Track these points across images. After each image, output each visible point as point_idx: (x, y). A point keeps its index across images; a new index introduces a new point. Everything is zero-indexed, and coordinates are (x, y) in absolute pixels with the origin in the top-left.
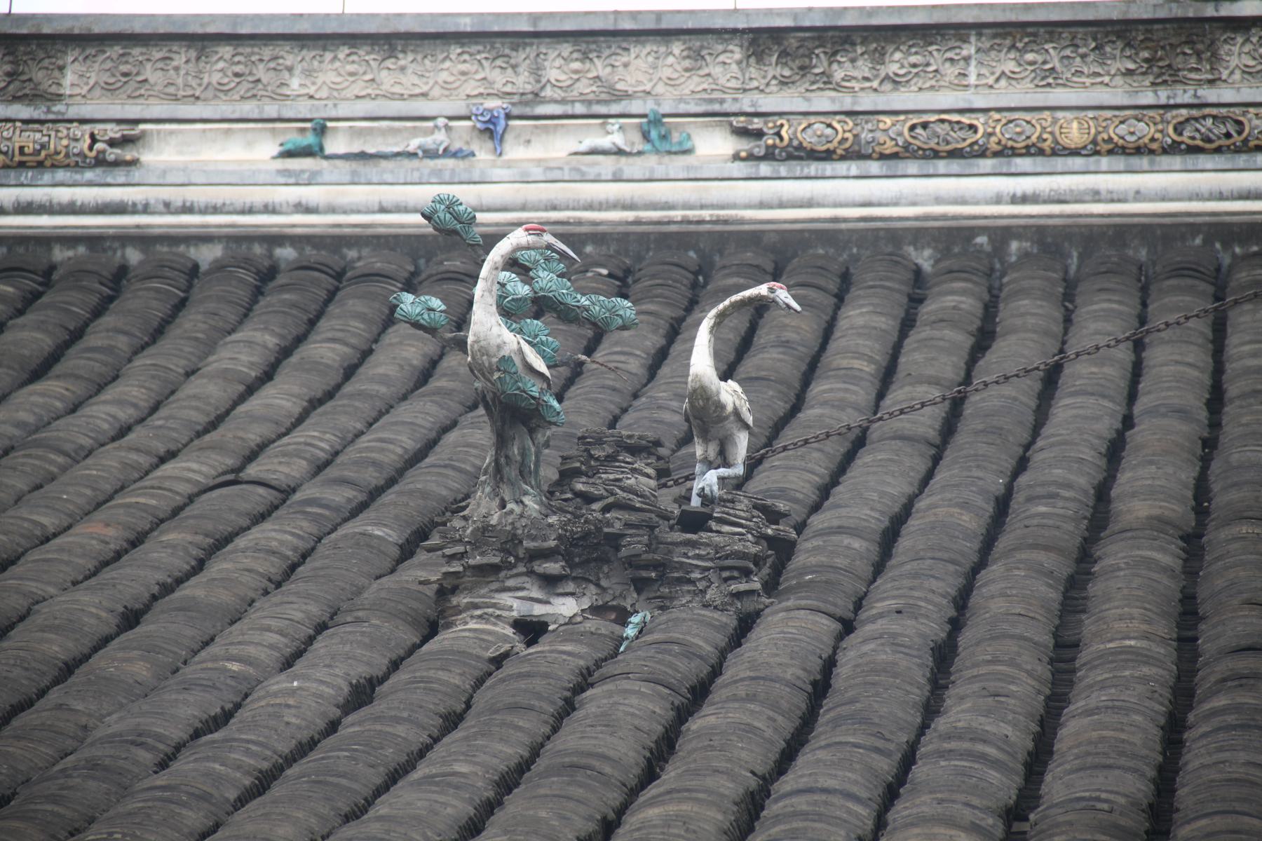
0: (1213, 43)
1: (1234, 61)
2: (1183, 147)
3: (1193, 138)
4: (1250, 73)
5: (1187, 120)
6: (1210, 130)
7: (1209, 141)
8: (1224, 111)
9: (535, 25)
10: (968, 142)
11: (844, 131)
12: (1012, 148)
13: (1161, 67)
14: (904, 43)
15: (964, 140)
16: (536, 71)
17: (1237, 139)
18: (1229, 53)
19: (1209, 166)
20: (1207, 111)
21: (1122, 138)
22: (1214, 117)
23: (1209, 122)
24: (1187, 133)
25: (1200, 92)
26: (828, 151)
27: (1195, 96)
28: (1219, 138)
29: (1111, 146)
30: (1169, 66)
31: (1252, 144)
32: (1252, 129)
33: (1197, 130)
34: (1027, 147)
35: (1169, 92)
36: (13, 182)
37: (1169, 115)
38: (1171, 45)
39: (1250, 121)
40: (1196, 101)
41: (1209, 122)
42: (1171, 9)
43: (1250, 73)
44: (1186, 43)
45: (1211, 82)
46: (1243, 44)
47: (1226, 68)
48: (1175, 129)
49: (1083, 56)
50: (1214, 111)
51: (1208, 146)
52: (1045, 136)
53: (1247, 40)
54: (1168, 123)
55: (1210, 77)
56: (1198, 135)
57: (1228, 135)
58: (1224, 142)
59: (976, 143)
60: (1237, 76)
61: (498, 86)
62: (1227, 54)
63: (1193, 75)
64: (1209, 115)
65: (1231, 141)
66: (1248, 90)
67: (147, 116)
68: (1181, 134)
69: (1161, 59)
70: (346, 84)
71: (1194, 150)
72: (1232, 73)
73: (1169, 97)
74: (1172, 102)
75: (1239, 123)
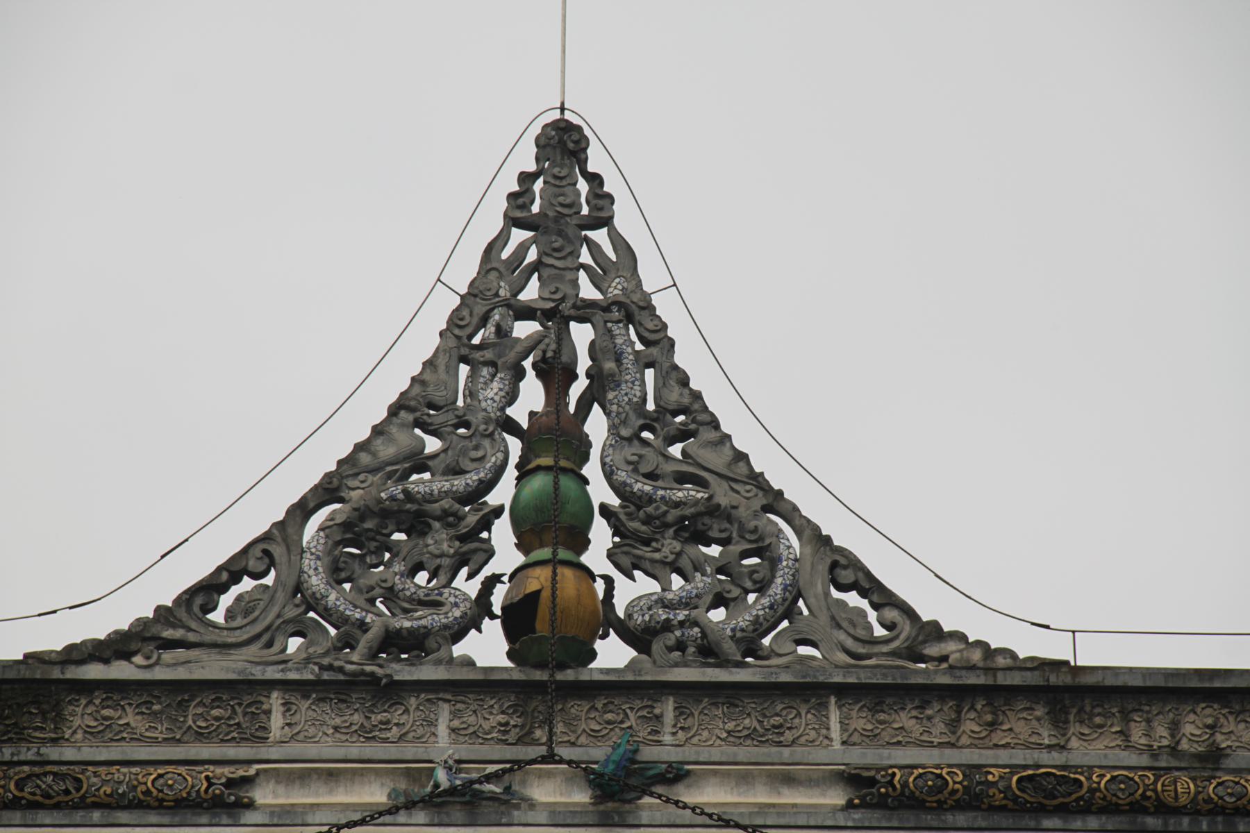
0: (58, 704)
1: (77, 722)
2: (24, 802)
3: (33, 794)
4: (91, 733)
5: (29, 777)
6: (50, 787)
7: (49, 797)
8: (64, 768)
9: (1073, 678)
10: (1074, 796)
11: (955, 783)
12: (1117, 804)
13: (8, 726)
14: (97, 697)
15: (1070, 794)
16: (1174, 727)
17: (75, 795)
18: (73, 714)
19: (47, 821)
20: (48, 768)
21: (1221, 798)
22: (55, 774)
23: (50, 779)
24: (27, 789)
25: (43, 750)
26: (938, 802)
27: (38, 753)
28: (58, 794)
29: (1212, 806)
30: (15, 724)
31: (89, 800)
32: (90, 786)
33: (38, 786)
34: (1131, 804)
35: (13, 750)
36: (17, 822)
37: (11, 772)
38: (18, 705)
39: (88, 778)
40: (39, 759)
41: (50, 779)
42: (19, 671)
43: (91, 733)
44: (33, 703)
45: (54, 741)
46: (86, 706)
47: (70, 728)
48: (17, 784)
49: (1038, 719)
50: (55, 769)
51: (47, 802)
52: (1149, 793)
53: (90, 702)
54: (11, 778)
55: (53, 736)
56: (38, 792)
57: (67, 792)
58: (62, 798)
59: (1081, 798)
60: (79, 736)
61: (916, 734)
62: (71, 715)
63: (37, 734)
64: (50, 773)
65: (70, 797)
66: (88, 749)
67: (259, 757)
68: (22, 790)
69: (8, 718)
70: (101, 728)
71: (34, 806)
72: (75, 732)
73: (13, 755)
74: (15, 758)
75: (78, 781)
